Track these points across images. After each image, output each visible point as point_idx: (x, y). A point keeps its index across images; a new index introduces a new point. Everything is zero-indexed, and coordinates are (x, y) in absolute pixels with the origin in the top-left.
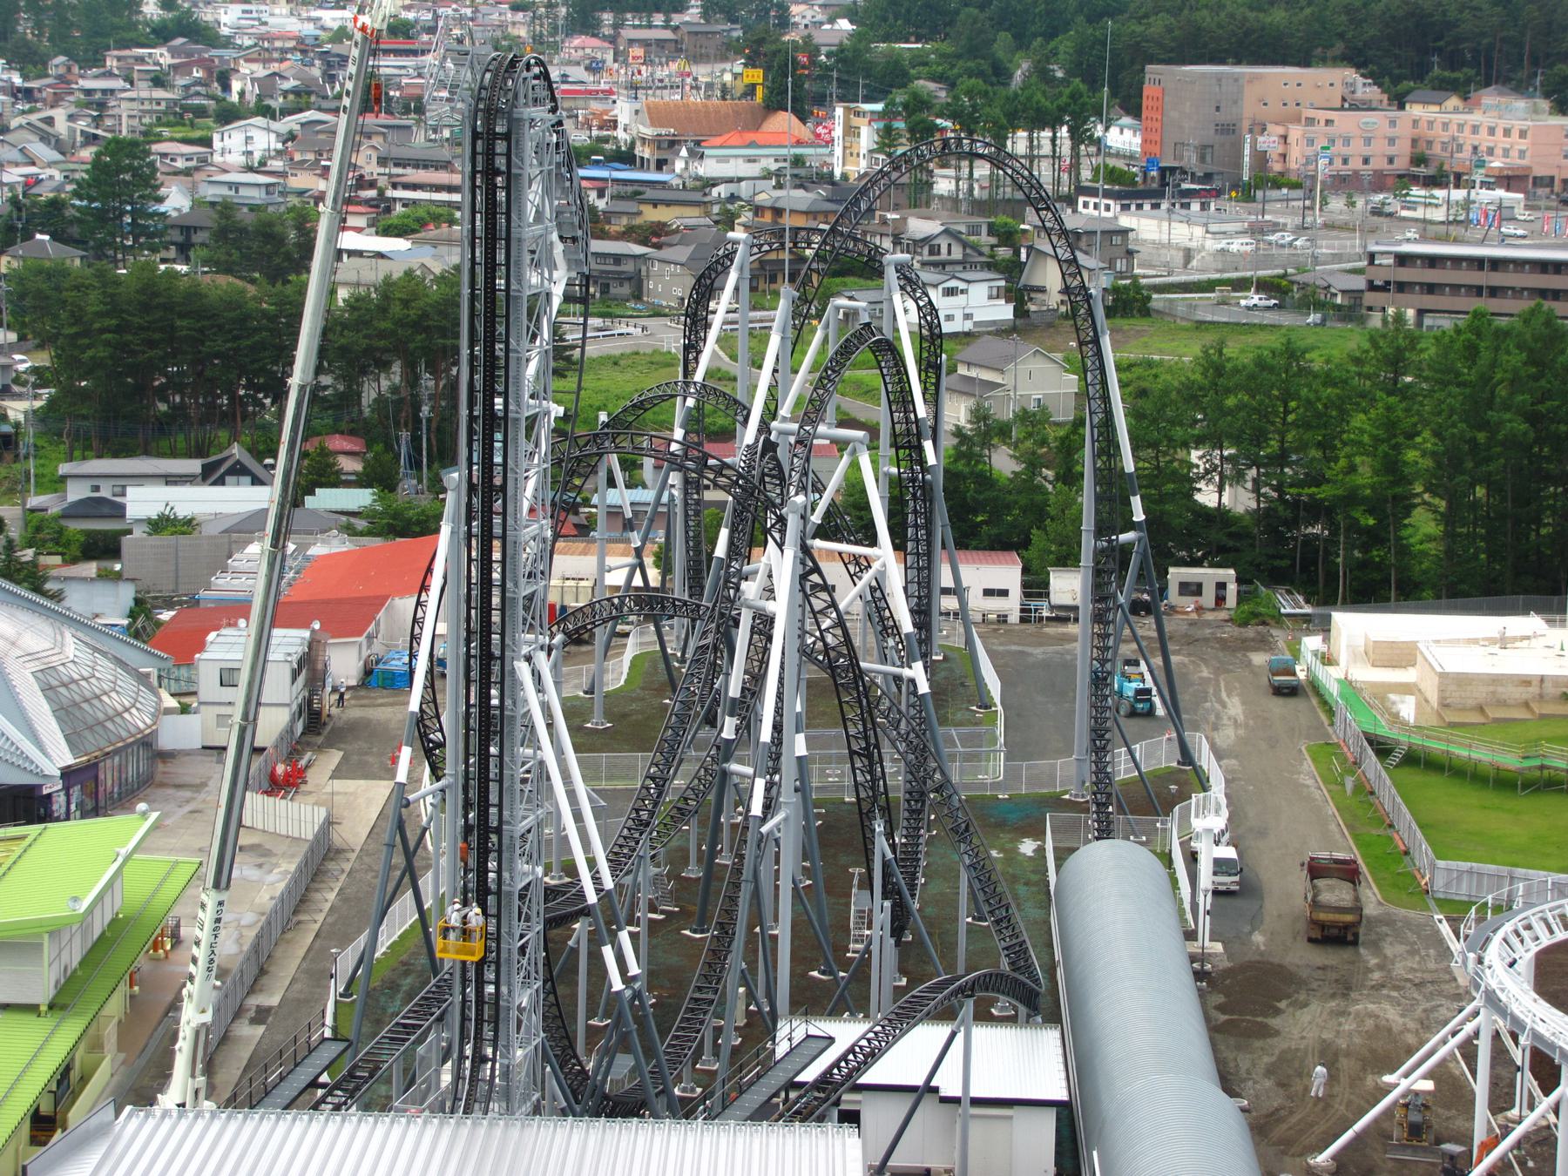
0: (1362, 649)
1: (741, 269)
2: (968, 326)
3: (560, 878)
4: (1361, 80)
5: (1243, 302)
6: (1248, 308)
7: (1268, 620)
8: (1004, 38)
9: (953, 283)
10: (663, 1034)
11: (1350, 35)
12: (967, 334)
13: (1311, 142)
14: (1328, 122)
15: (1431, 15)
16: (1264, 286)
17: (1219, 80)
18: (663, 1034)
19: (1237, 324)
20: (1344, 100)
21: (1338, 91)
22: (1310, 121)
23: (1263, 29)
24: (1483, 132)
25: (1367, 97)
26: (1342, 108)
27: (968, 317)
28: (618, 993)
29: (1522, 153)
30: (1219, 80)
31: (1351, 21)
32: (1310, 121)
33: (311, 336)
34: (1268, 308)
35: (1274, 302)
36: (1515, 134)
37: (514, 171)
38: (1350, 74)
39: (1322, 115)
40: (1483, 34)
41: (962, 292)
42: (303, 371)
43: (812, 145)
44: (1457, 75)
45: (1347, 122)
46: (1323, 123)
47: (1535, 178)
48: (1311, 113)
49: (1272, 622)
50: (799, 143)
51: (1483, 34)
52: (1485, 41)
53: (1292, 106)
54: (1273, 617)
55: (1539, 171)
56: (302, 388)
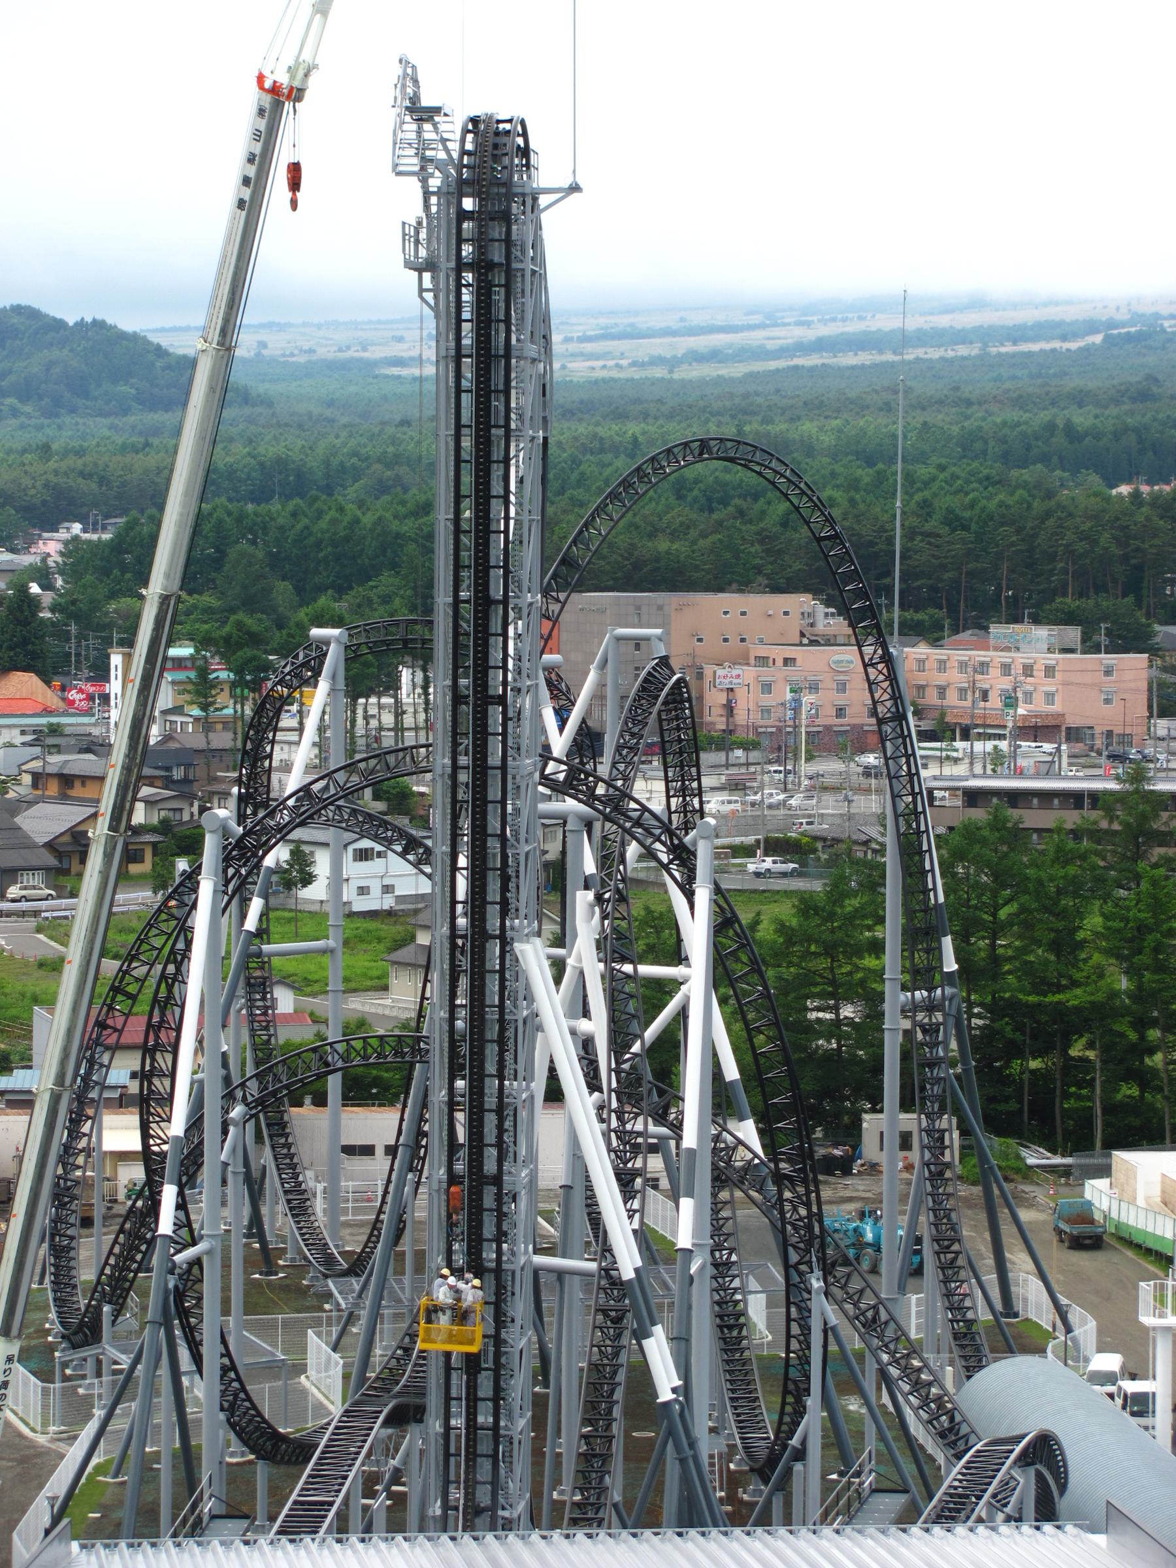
0: (1159, 1199)
1: (334, 677)
2: (388, 903)
3: (243, 1454)
4: (821, 609)
5: (751, 867)
6: (758, 874)
7: (1012, 1175)
8: (283, 590)
9: (366, 843)
10: (629, 1516)
11: (768, 569)
12: (390, 913)
13: (767, 688)
14: (787, 661)
15: (871, 544)
16: (774, 847)
17: (638, 608)
18: (629, 1516)
19: (755, 891)
20: (802, 635)
21: (795, 625)
22: (762, 661)
23: (658, 560)
24: (995, 672)
25: (830, 631)
26: (801, 644)
27: (388, 889)
28: (666, 1404)
29: (1050, 697)
30: (638, 608)
31: (768, 552)
32: (762, 661)
33: (180, 524)
34: (784, 875)
35: (792, 865)
36: (1039, 673)
37: (515, 265)
38: (803, 602)
39: (779, 653)
40: (943, 567)
41: (379, 855)
42: (167, 576)
43: (65, 714)
44: (920, 616)
45: (812, 660)
46: (780, 662)
47: (1068, 729)
48: (762, 651)
49: (1018, 1177)
50: (48, 712)
51: (943, 567)
52: (947, 576)
53: (734, 641)
54: (1018, 1171)
55: (1072, 721)
56: (165, 599)
